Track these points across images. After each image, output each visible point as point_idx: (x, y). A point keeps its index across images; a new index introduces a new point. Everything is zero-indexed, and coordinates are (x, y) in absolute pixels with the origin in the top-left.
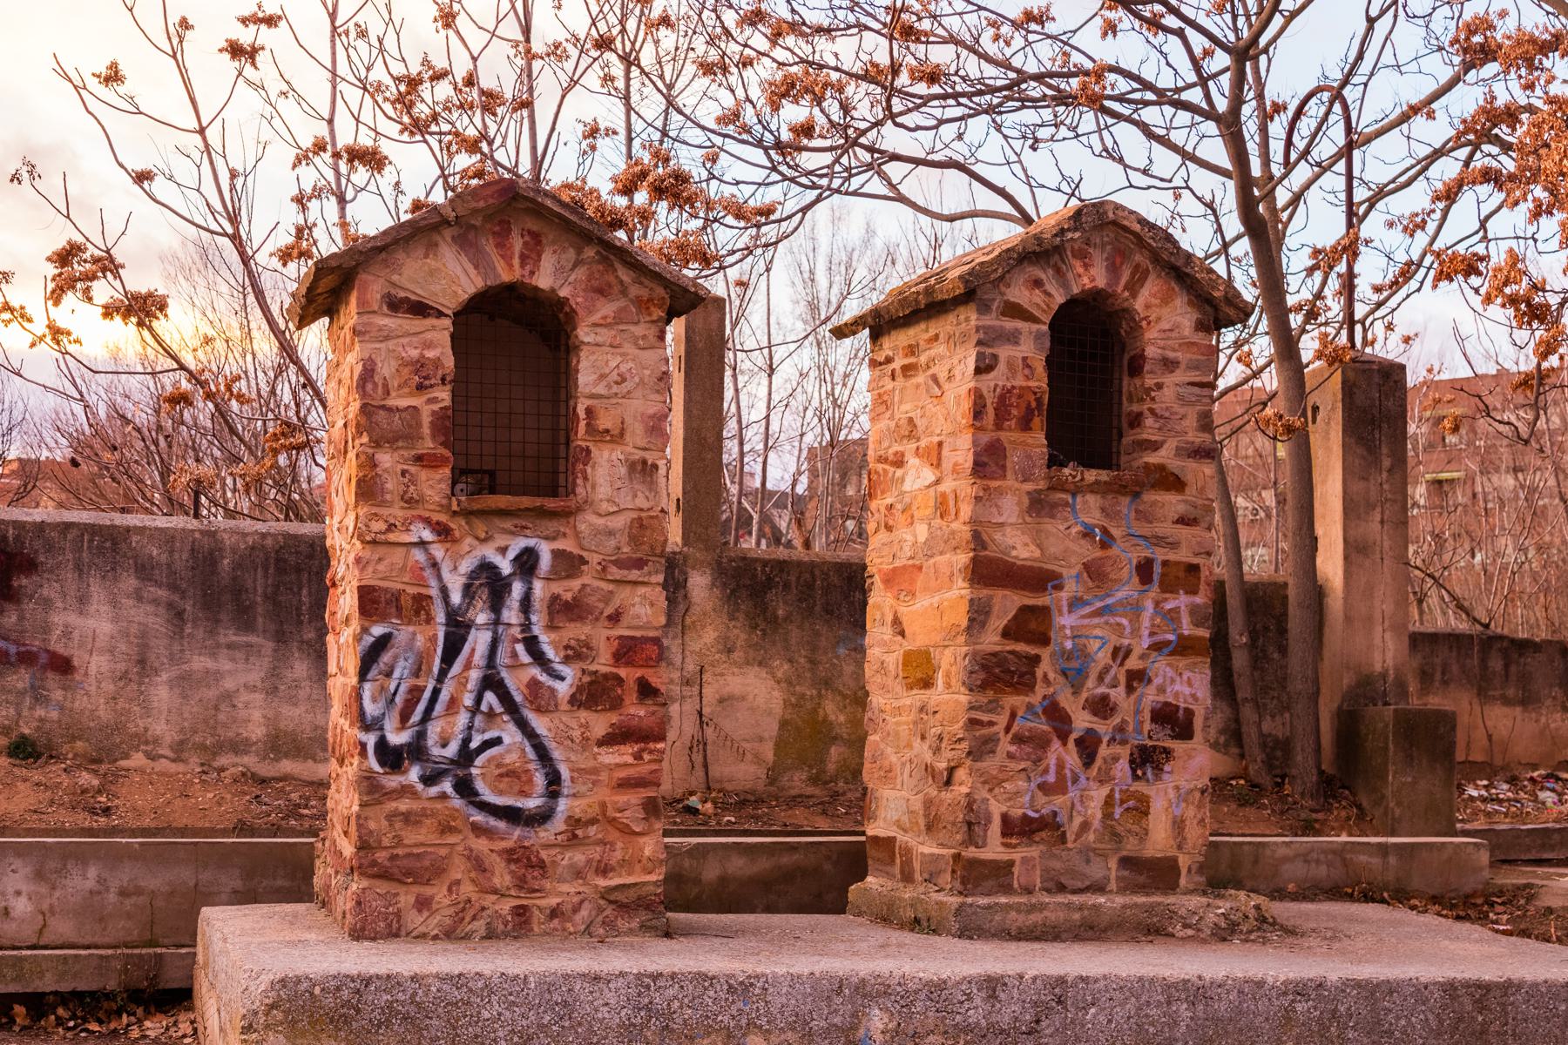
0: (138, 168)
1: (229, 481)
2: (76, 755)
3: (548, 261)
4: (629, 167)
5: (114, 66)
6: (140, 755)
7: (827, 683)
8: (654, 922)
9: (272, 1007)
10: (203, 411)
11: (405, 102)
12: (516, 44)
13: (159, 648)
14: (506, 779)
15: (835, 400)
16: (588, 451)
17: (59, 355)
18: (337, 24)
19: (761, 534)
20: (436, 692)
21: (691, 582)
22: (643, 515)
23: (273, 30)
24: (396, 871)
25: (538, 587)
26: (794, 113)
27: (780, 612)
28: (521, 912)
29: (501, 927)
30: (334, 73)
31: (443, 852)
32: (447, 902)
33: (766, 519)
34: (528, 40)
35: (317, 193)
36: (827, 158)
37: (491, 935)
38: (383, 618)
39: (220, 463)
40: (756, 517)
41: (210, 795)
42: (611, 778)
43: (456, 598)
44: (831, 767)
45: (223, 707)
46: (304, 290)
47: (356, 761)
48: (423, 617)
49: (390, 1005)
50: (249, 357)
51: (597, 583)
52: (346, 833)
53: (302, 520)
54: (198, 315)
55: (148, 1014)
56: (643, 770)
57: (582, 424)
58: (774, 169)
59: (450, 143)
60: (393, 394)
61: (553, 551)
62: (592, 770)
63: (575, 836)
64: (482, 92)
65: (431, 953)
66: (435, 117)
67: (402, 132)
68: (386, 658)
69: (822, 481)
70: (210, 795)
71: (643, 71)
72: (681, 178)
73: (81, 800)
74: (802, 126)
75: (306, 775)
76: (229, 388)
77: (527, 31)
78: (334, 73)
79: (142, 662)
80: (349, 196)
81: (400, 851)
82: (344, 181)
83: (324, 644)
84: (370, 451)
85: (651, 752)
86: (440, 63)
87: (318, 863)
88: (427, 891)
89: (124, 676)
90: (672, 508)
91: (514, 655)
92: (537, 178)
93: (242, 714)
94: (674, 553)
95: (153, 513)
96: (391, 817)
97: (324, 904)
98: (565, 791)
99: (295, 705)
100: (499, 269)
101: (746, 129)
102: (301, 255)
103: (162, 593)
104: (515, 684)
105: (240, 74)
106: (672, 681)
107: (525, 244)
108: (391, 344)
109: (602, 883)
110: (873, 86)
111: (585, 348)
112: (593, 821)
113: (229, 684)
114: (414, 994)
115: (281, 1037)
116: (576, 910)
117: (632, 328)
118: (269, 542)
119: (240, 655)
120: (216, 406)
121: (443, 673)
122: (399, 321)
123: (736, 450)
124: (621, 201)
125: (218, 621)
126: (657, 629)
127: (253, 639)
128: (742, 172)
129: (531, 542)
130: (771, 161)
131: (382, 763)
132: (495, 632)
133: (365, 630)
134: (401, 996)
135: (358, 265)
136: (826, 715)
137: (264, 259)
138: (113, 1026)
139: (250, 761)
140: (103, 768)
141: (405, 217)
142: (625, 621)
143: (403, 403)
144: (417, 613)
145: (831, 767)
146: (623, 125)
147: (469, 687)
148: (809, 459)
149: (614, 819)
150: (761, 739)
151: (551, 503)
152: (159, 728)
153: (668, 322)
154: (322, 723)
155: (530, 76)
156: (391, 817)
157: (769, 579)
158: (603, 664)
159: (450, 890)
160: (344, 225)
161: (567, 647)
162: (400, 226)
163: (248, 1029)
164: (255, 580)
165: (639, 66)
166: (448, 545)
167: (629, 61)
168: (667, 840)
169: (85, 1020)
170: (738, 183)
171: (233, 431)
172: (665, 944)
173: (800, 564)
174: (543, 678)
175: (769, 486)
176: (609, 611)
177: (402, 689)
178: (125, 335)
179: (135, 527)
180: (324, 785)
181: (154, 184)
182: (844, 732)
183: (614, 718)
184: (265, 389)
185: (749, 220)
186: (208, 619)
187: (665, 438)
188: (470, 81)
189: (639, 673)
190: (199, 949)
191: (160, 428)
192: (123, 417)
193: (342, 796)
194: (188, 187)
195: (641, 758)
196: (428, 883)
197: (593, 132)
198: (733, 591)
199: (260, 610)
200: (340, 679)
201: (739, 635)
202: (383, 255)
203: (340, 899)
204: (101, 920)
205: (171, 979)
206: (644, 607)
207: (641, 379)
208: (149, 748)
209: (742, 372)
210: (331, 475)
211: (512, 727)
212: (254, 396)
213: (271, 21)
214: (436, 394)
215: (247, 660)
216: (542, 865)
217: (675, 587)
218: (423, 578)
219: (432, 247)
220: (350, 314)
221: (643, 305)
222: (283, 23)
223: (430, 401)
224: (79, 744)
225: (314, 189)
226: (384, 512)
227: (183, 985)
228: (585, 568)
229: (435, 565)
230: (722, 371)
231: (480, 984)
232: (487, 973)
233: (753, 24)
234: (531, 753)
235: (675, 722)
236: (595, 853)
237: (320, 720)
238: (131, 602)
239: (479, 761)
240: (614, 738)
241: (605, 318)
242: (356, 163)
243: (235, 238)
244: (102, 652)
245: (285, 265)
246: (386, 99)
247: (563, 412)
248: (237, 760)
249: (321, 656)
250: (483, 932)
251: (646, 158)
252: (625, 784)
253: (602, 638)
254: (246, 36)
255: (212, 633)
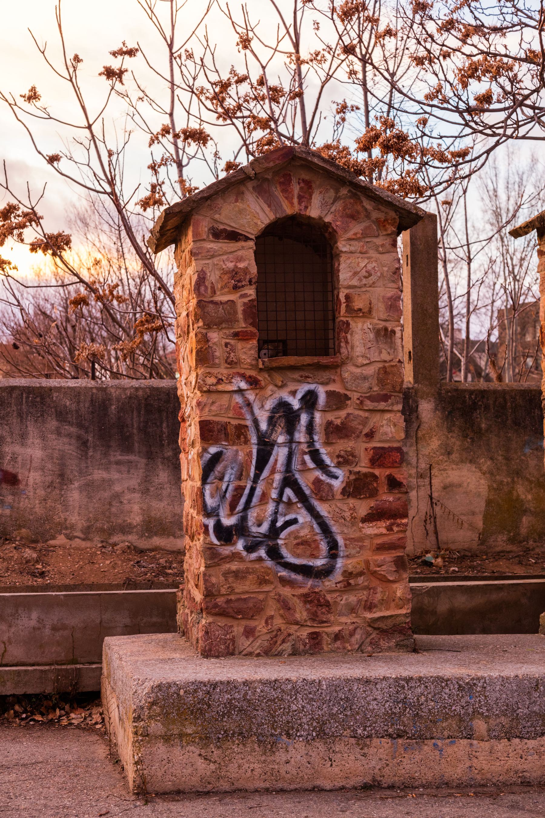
0: (50, 154)
1: (113, 352)
2: (22, 538)
3: (316, 199)
4: (368, 132)
5: (33, 89)
6: (62, 536)
7: (518, 473)
8: (405, 642)
9: (153, 704)
10: (95, 308)
11: (218, 98)
12: (291, 54)
13: (72, 465)
14: (301, 547)
15: (515, 277)
16: (348, 324)
17: (4, 278)
18: (174, 51)
19: (467, 371)
20: (253, 490)
21: (421, 408)
22: (387, 365)
23: (133, 58)
24: (230, 610)
25: (318, 416)
26: (477, 87)
27: (483, 425)
28: (315, 637)
29: (302, 647)
30: (172, 83)
31: (261, 597)
32: (265, 630)
33: (470, 360)
34: (297, 51)
35: (164, 162)
36: (502, 116)
37: (295, 653)
38: (216, 442)
39: (107, 341)
40: (463, 360)
41: (108, 562)
42: (372, 544)
43: (264, 426)
44: (524, 531)
45: (114, 503)
46: (158, 228)
47: (202, 537)
48: (243, 440)
49: (230, 701)
50: (123, 271)
51: (357, 412)
52: (197, 586)
53: (161, 378)
54: (91, 245)
55: (73, 709)
56: (393, 538)
57: (343, 306)
58: (467, 125)
59: (250, 123)
60: (218, 293)
61: (327, 392)
62: (359, 540)
63: (349, 584)
64: (270, 89)
65: (256, 666)
66: (239, 107)
67: (218, 118)
68: (219, 468)
69: (509, 332)
70: (108, 562)
71: (374, 67)
72: (402, 138)
73: (27, 568)
74: (484, 96)
75: (169, 547)
76: (111, 292)
77: (296, 45)
78: (172, 83)
79: (62, 475)
80: (184, 162)
81: (233, 597)
82: (181, 152)
83: (178, 459)
84: (204, 331)
85: (398, 525)
86: (241, 72)
87: (179, 606)
88: (252, 623)
89: (51, 485)
90: (406, 358)
91: (304, 463)
92: (306, 142)
93: (127, 507)
94: (408, 388)
95: (67, 378)
96: (226, 574)
97: (184, 634)
98: (341, 554)
99: (161, 500)
100: (285, 207)
101: (445, 100)
102: (155, 203)
103: (73, 430)
104: (305, 482)
105: (113, 88)
106: (410, 476)
107: (301, 188)
108: (215, 260)
109: (369, 615)
110: (532, 65)
111: (343, 255)
112: (361, 574)
113: (117, 488)
114: (246, 694)
115: (159, 724)
116: (352, 634)
117: (374, 240)
118: (140, 393)
119: (124, 468)
120: (104, 305)
121: (257, 477)
122: (220, 245)
123: (448, 314)
124: (362, 156)
125: (109, 447)
126: (399, 441)
127: (132, 457)
128: (445, 129)
129: (312, 387)
130: (464, 119)
131: (219, 539)
132: (290, 448)
133: (205, 450)
134: (237, 696)
135: (192, 209)
136: (518, 496)
137: (132, 208)
138: (50, 717)
139: (132, 538)
140: (39, 545)
141: (222, 175)
142: (377, 437)
143: (225, 298)
144: (239, 437)
145: (524, 531)
146: (363, 102)
147: (275, 485)
148: (499, 318)
149: (375, 572)
150: (474, 513)
151: (324, 360)
152: (75, 518)
153: (398, 234)
154: (179, 512)
155: (300, 75)
156: (226, 574)
157: (474, 403)
158: (363, 467)
159: (267, 622)
160: (182, 182)
161: (338, 456)
162: (219, 183)
163: (137, 719)
164: (132, 419)
165: (372, 64)
166: (257, 391)
167: (365, 60)
168: (412, 585)
169: (33, 714)
170: (441, 137)
171: (114, 320)
172: (413, 657)
173: (495, 392)
174: (323, 477)
175: (472, 337)
176: (366, 430)
177: (230, 488)
178: (44, 261)
179: (55, 387)
180: (180, 553)
181: (60, 163)
182: (531, 506)
183: (373, 503)
184: (135, 291)
185: (449, 162)
186: (103, 446)
187: (400, 313)
188: (262, 82)
189: (388, 472)
190: (104, 665)
191: (68, 320)
192: (44, 313)
193: (194, 561)
194: (82, 165)
195: (392, 530)
196: (252, 618)
197: (343, 109)
198: (450, 413)
199: (136, 438)
200: (190, 483)
201: (455, 442)
202: (209, 202)
203: (195, 630)
204: (41, 646)
205: (87, 685)
206: (389, 427)
207: (381, 274)
208: (68, 532)
209: (450, 261)
210: (179, 344)
211: (304, 511)
212: (127, 297)
213: (131, 53)
214: (246, 292)
215: (129, 472)
216: (327, 604)
217: (410, 412)
218: (241, 414)
219: (240, 195)
220: (189, 242)
221: (381, 224)
222: (139, 54)
223: (242, 296)
224: (24, 530)
225: (162, 160)
226: (214, 371)
227: (95, 689)
228: (349, 402)
229: (249, 405)
230: (437, 264)
231: (289, 687)
232: (294, 678)
233: (448, 30)
234: (317, 529)
235: (414, 503)
236: (363, 595)
237: (177, 510)
238: (54, 437)
239: (283, 535)
240: (373, 516)
241: (355, 234)
242: (190, 140)
243: (113, 194)
244: (36, 469)
245: (145, 210)
246: (207, 98)
247: (330, 298)
248: (124, 538)
249: (177, 468)
250: (289, 651)
251: (379, 126)
252: (381, 548)
253: (362, 449)
254: (115, 64)
255: (106, 454)
